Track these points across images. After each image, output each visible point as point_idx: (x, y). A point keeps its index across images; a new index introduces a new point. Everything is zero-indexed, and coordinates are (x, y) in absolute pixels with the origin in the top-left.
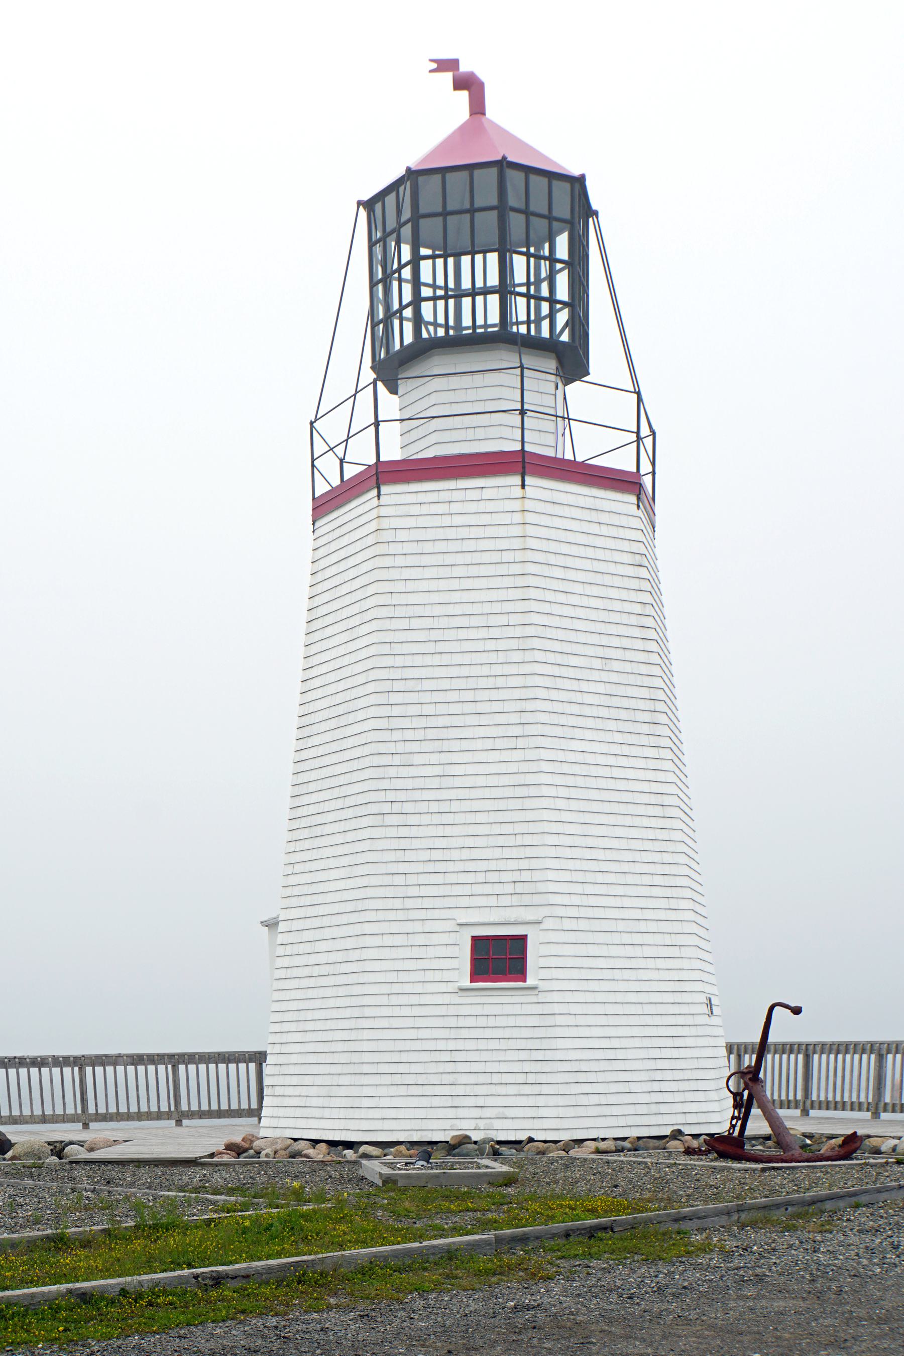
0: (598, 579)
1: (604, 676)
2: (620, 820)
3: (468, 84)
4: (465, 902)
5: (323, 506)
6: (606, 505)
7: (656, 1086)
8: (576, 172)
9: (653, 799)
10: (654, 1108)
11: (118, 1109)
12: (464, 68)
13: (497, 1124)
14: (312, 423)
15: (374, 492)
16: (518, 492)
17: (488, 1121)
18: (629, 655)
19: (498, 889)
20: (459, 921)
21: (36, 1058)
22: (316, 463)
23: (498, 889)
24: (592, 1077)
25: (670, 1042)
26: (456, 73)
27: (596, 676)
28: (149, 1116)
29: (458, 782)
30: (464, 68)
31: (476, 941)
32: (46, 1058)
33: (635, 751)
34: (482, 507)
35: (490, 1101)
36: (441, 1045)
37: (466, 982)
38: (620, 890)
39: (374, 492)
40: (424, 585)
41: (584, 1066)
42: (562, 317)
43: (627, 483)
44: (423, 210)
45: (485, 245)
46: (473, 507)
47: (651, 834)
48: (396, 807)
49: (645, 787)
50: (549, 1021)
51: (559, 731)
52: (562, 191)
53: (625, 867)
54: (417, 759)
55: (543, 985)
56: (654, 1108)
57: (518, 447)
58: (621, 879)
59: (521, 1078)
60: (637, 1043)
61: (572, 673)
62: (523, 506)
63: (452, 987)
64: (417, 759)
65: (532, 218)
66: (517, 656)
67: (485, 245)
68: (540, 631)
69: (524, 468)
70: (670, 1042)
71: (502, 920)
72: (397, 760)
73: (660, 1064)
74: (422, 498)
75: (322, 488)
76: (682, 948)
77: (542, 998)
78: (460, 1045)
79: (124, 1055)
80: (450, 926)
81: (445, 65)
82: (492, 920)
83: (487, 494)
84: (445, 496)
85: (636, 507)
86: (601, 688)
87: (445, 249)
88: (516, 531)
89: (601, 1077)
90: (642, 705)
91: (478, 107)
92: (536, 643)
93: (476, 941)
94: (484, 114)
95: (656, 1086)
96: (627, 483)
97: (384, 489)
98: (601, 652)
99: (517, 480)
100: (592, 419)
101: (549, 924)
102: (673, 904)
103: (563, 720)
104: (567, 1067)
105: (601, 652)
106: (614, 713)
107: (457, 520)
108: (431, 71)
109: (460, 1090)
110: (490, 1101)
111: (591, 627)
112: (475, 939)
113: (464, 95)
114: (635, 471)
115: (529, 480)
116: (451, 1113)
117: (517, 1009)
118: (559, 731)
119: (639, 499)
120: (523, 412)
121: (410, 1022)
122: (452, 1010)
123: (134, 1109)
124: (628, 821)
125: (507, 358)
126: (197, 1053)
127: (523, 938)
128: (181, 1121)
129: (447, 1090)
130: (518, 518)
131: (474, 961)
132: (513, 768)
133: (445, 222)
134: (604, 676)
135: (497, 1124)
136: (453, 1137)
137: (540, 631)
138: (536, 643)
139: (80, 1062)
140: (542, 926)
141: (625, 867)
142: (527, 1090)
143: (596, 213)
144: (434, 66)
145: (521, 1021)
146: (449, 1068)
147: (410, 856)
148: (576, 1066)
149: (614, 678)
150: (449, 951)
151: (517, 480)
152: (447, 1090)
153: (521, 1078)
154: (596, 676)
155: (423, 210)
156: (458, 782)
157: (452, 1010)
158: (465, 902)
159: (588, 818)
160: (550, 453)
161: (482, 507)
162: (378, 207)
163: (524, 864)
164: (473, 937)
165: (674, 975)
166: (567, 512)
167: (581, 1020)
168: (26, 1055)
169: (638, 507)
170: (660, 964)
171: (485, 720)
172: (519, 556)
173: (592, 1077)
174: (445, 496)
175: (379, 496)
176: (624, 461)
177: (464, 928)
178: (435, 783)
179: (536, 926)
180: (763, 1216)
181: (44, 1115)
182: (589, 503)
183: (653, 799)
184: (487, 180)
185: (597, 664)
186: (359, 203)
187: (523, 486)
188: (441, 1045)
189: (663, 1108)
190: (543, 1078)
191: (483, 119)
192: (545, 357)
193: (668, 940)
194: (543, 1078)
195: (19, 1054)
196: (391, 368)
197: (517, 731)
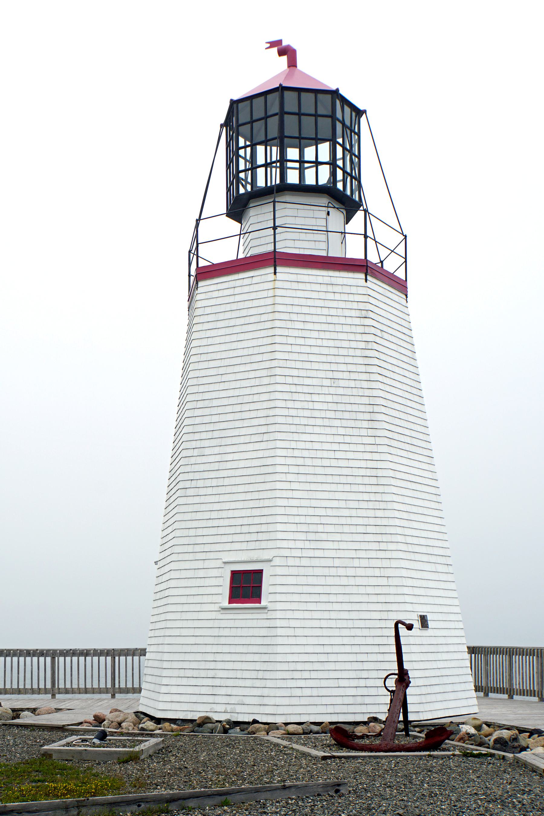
0: (331, 328)
1: (332, 391)
2: (340, 488)
3: (287, 52)
4: (228, 547)
6: (340, 281)
7: (362, 683)
8: (334, 88)
9: (369, 472)
10: (359, 700)
11: (133, 685)
12: (284, 44)
13: (239, 709)
16: (272, 277)
17: (233, 706)
18: (353, 376)
19: (248, 537)
20: (224, 560)
21: (83, 650)
23: (248, 537)
24: (306, 675)
25: (376, 649)
26: (280, 47)
27: (325, 390)
28: (93, 691)
29: (229, 465)
30: (284, 44)
31: (234, 573)
32: (90, 650)
33: (354, 440)
34: (252, 288)
35: (235, 691)
36: (209, 649)
37: (226, 604)
38: (338, 537)
40: (218, 340)
41: (299, 667)
45: (291, 137)
46: (246, 289)
47: (366, 497)
48: (194, 484)
49: (363, 464)
50: (273, 632)
51: (293, 428)
53: (343, 521)
54: (207, 451)
55: (271, 606)
56: (359, 700)
57: (271, 248)
58: (339, 529)
59: (254, 675)
60: (348, 649)
61: (306, 389)
62: (274, 285)
63: (216, 607)
64: (207, 451)
66: (266, 381)
67: (291, 137)
68: (282, 363)
69: (275, 262)
70: (376, 649)
71: (249, 559)
72: (196, 452)
73: (366, 666)
74: (220, 287)
76: (390, 579)
77: (271, 615)
78: (220, 649)
79: (139, 649)
80: (219, 563)
81: (273, 44)
82: (240, 559)
83: (255, 280)
84: (232, 284)
85: (364, 280)
86: (329, 398)
87: (251, 141)
88: (270, 301)
89: (314, 675)
90: (362, 408)
91: (292, 63)
92: (278, 371)
93: (234, 573)
95: (362, 683)
98: (330, 374)
99: (272, 270)
101: (277, 561)
102: (383, 546)
103: (296, 421)
104: (285, 667)
105: (330, 374)
106: (339, 415)
107: (238, 298)
108: (266, 48)
109: (217, 682)
110: (235, 691)
111: (324, 359)
112: (233, 573)
113: (285, 58)
114: (364, 258)
115: (279, 269)
116: (210, 699)
117: (254, 623)
118: (293, 428)
120: (275, 228)
121: (191, 632)
122: (216, 624)
123: (15, 686)
124: (347, 488)
125: (324, 200)
126: (12, 650)
127: (260, 572)
128: (55, 695)
129: (210, 682)
130: (271, 293)
131: (232, 588)
132: (260, 454)
133: (316, 134)
134: (332, 391)
135: (239, 709)
136: (200, 718)
137: (282, 363)
138: (278, 371)
139: (113, 653)
140: (272, 563)
141: (343, 521)
142: (258, 683)
144: (269, 45)
145: (256, 632)
146: (212, 665)
147: (199, 516)
148: (292, 666)
149: (340, 391)
150: (279, 580)
151: (272, 270)
152: (210, 682)
153: (254, 675)
154: (325, 390)
156: (229, 465)
157: (216, 624)
158: (228, 547)
159: (313, 487)
160: (324, 254)
161: (252, 288)
163: (264, 520)
164: (232, 571)
165: (382, 599)
166: (308, 287)
167: (299, 632)
168: (77, 648)
170: (370, 590)
171: (246, 423)
172: (271, 317)
173: (306, 675)
174: (232, 284)
177: (227, 565)
178: (216, 466)
179: (269, 563)
181: (86, 688)
182: (327, 280)
183: (369, 472)
184: (274, 99)
185: (327, 382)
187: (275, 273)
188: (209, 649)
189: (367, 700)
190: (268, 675)
192: (301, 196)
193: (377, 572)
194: (268, 675)
195: (73, 647)
197: (263, 429)
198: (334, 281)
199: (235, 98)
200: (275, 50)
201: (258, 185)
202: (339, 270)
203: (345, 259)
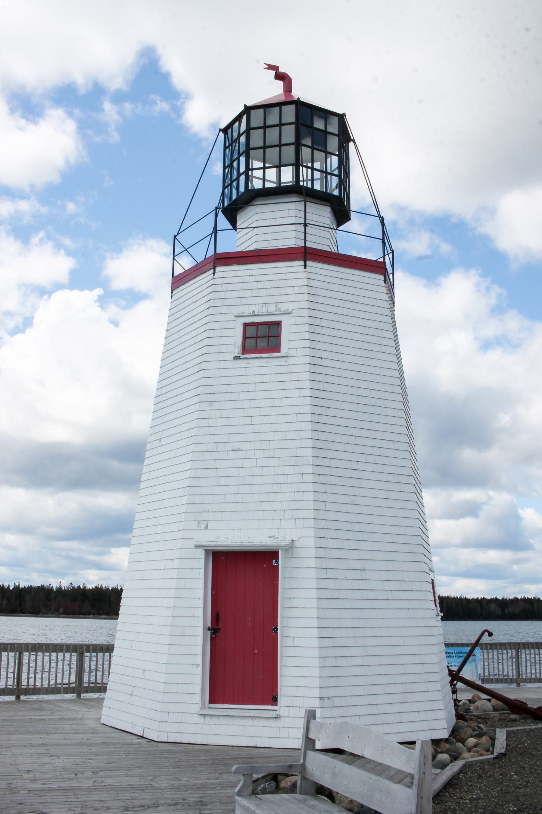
3: (281, 77)
5: (178, 281)
8: (340, 112)
12: (281, 70)
14: (175, 237)
15: (212, 271)
39: (212, 271)
42: (335, 181)
43: (377, 267)
44: (252, 125)
52: (335, 121)
69: (305, 256)
75: (179, 271)
81: (270, 67)
91: (288, 88)
94: (291, 92)
96: (377, 267)
97: (218, 269)
100: (356, 237)
113: (281, 83)
115: (309, 263)
119: (385, 277)
120: (305, 225)
127: (278, 324)
144: (267, 67)
155: (252, 125)
162: (229, 131)
169: (385, 282)
175: (214, 274)
176: (373, 254)
180: (450, 653)
182: (256, 272)
186: (220, 130)
187: (305, 267)
191: (292, 94)
196: (109, 648)
198: (262, 272)
199: (248, 105)
202: (329, 263)
203: (338, 254)
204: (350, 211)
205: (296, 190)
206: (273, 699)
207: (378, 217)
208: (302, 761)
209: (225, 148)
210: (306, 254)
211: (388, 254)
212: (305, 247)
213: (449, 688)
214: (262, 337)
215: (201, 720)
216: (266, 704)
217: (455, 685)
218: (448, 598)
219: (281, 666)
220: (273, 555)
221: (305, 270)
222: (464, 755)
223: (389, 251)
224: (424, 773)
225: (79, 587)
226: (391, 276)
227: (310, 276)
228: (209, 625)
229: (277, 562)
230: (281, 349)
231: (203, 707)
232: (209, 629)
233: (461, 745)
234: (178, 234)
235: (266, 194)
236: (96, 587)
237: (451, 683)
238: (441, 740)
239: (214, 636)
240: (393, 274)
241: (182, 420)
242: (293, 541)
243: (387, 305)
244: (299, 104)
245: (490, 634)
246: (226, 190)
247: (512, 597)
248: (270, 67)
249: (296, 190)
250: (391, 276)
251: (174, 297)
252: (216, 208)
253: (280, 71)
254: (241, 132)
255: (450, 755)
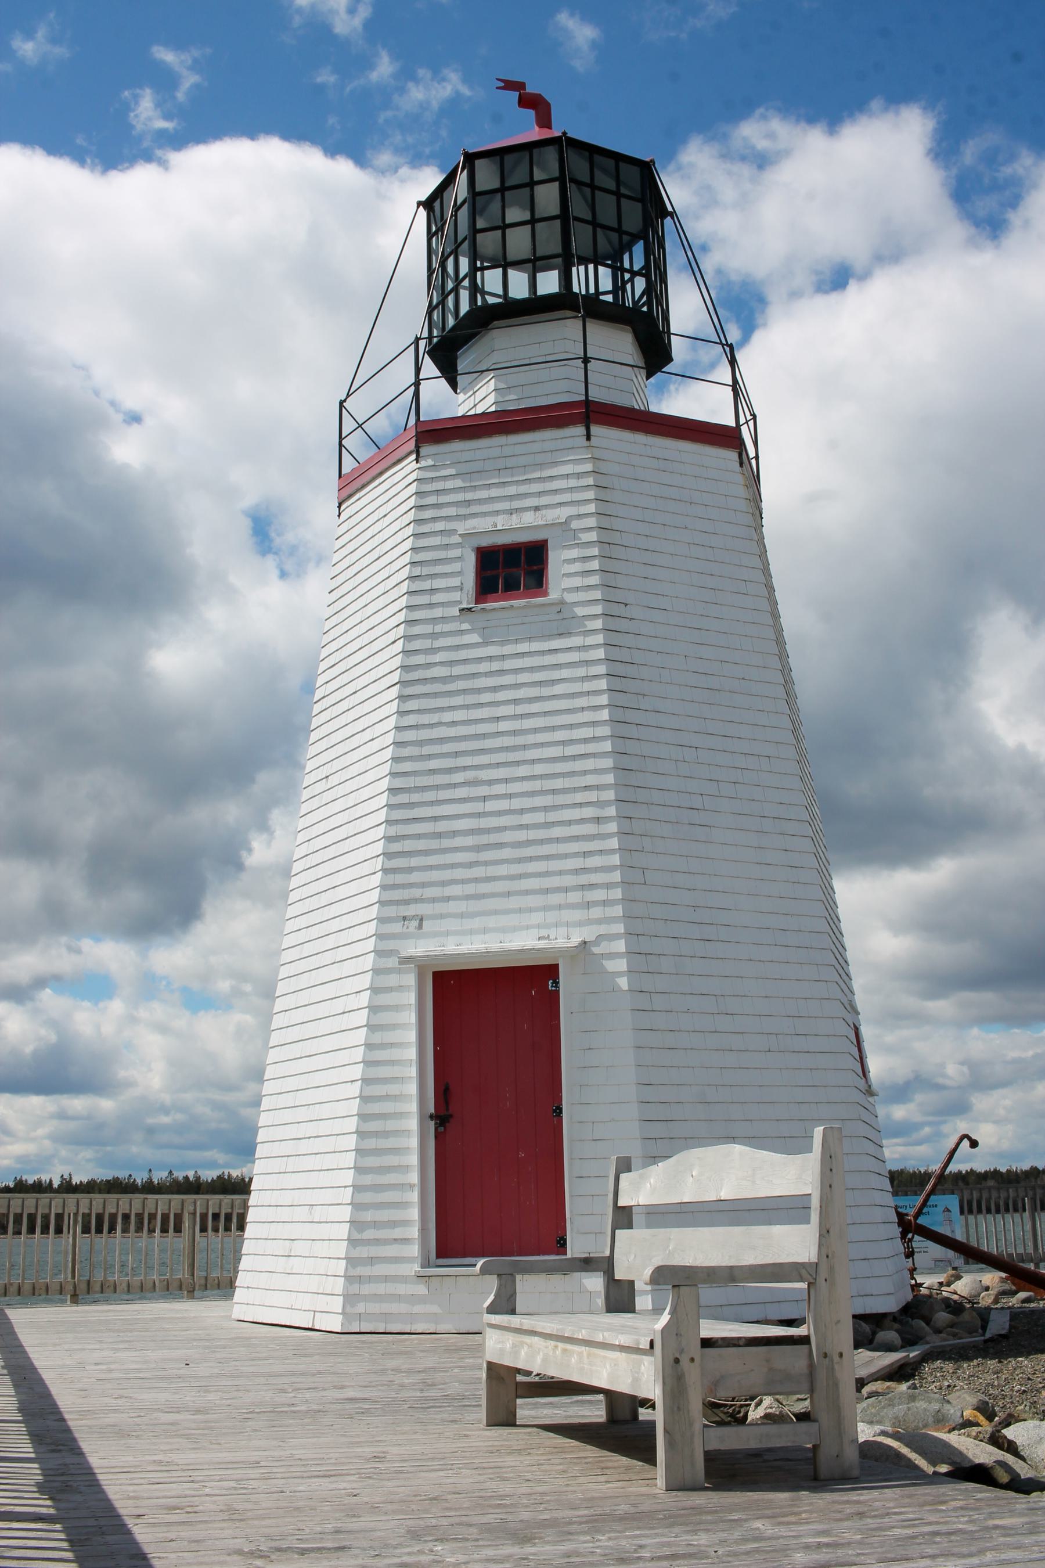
12: (529, 89)
14: (341, 404)
16: (583, 441)
22: (343, 442)
30: (529, 89)
52: (630, 175)
57: (584, 398)
65: (597, 192)
81: (509, 85)
91: (544, 120)
96: (727, 438)
115: (595, 429)
120: (586, 360)
143: (673, 214)
151: (580, 430)
162: (437, 205)
182: (496, 452)
186: (419, 204)
187: (588, 437)
198: (507, 451)
200: (516, 95)
201: (557, 290)
204: (669, 334)
205: (563, 302)
206: (558, 1242)
207: (721, 343)
208: (607, 1253)
209: (430, 235)
210: (590, 413)
211: (747, 422)
212: (587, 402)
213: (899, 1246)
214: (510, 569)
215: (421, 1289)
216: (544, 1254)
217: (911, 1240)
218: (901, 1172)
219: (571, 1196)
220: (551, 971)
221: (586, 443)
222: (928, 1338)
223: (749, 417)
224: (830, 1186)
225: (187, 1178)
226: (753, 462)
227: (598, 454)
228: (431, 1109)
229: (556, 983)
230: (550, 591)
231: (426, 1264)
232: (431, 1117)
233: (923, 1324)
234: (348, 396)
235: (512, 311)
236: (219, 1177)
237: (903, 1235)
238: (884, 1315)
239: (441, 1129)
240: (757, 457)
241: (367, 735)
242: (585, 942)
243: (748, 519)
244: (565, 144)
245: (974, 1144)
246: (435, 312)
247: (1026, 1166)
248: (509, 85)
249: (563, 302)
250: (753, 462)
251: (344, 516)
252: (417, 340)
253: (528, 90)
254: (459, 240)
255: (903, 1339)
